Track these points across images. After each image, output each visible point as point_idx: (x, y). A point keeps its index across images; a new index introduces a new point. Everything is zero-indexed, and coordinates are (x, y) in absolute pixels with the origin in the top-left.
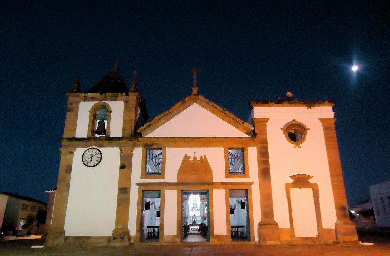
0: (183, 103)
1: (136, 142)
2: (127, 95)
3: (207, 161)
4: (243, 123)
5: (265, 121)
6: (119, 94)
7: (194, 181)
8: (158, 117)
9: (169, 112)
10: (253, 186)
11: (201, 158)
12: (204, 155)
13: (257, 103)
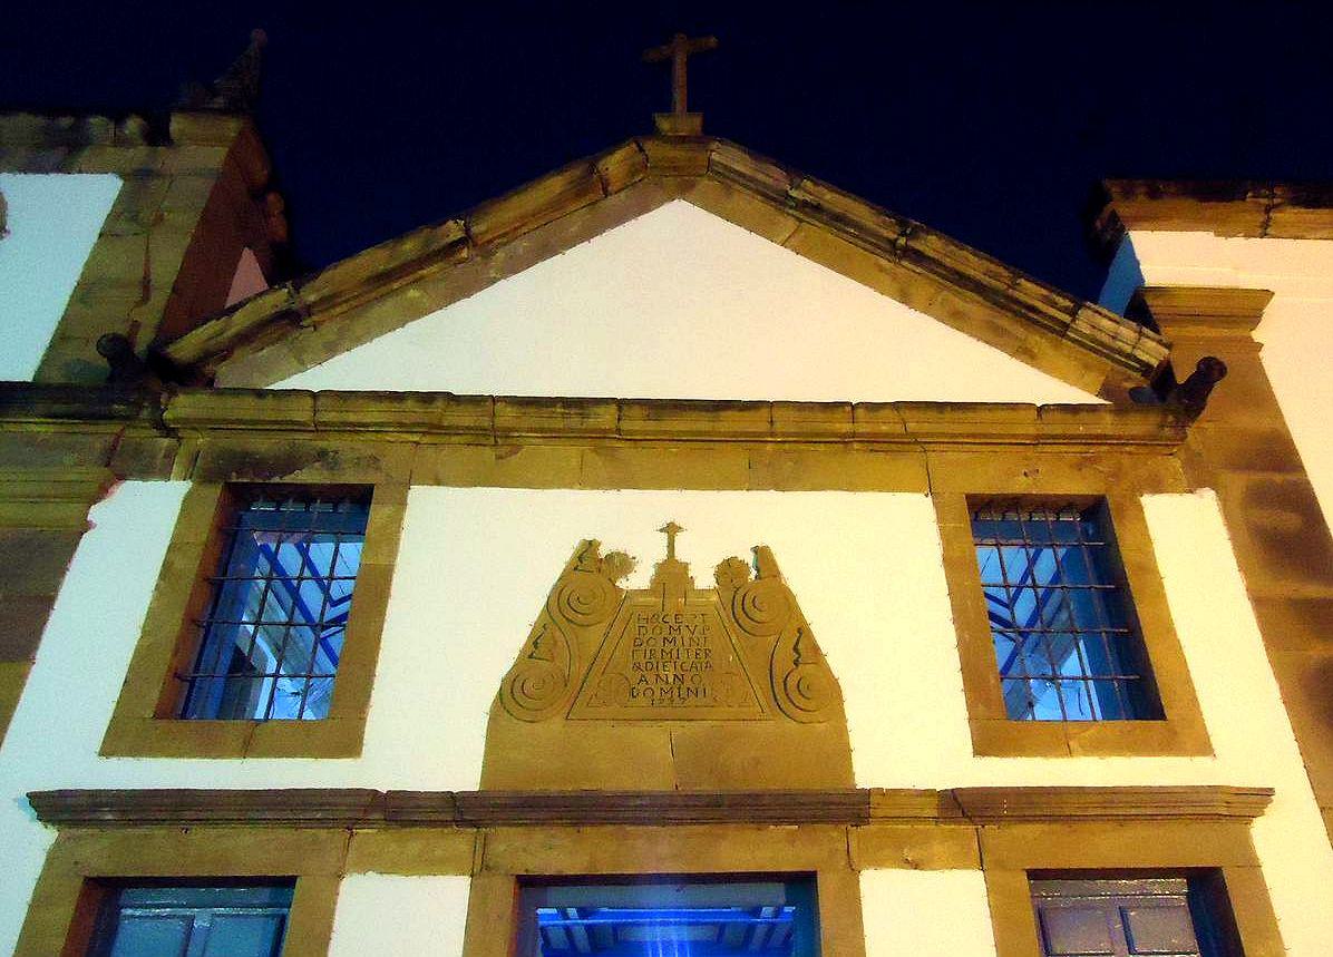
0: (579, 191)
1: (141, 434)
2: (157, 135)
3: (787, 601)
4: (1073, 314)
5: (1244, 308)
6: (97, 123)
7: (659, 781)
8: (373, 259)
9: (467, 230)
10: (1264, 834)
11: (729, 571)
12: (756, 550)
13: (1154, 194)
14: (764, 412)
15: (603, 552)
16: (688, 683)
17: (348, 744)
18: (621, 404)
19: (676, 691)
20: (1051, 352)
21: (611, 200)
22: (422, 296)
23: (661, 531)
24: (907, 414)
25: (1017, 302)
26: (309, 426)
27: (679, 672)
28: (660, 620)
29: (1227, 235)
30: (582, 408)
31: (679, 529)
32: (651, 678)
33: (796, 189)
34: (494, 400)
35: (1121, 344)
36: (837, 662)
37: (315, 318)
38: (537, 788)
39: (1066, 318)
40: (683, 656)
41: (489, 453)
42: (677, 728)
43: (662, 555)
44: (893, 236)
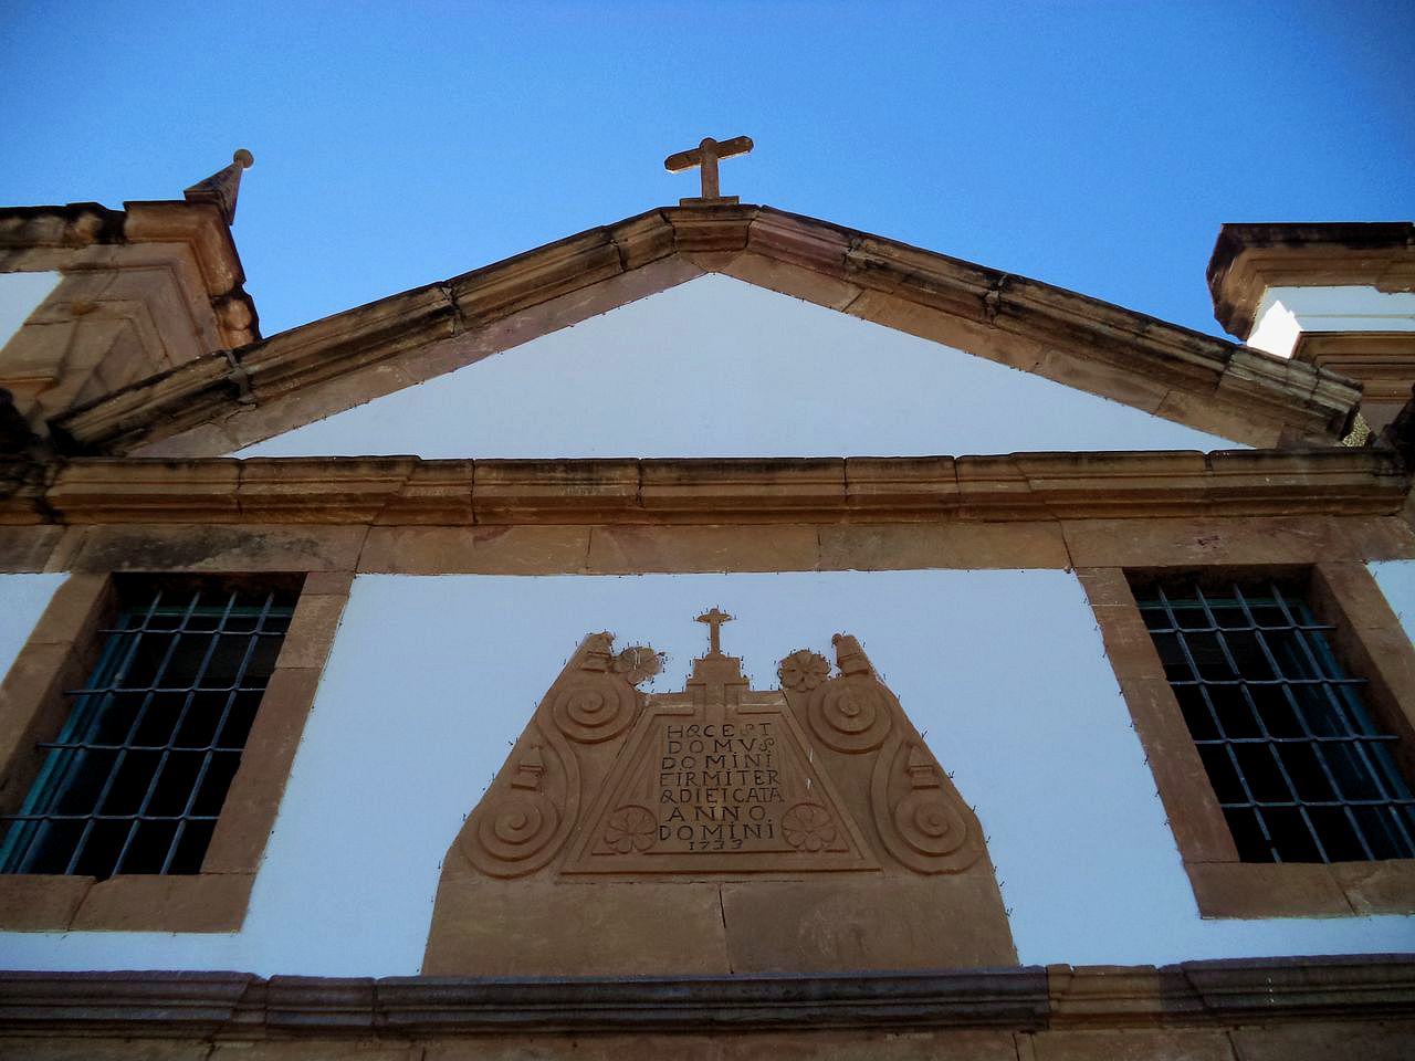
9: (454, 299)
11: (799, 668)
12: (837, 640)
14: (836, 472)
15: (617, 648)
16: (744, 818)
17: (228, 915)
18: (642, 465)
19: (726, 831)
20: (1202, 409)
21: (629, 276)
22: (393, 373)
23: (699, 620)
24: (1027, 467)
25: (1150, 352)
26: (230, 503)
27: (731, 804)
28: (701, 732)
29: (1391, 291)
30: (591, 471)
31: (725, 617)
32: (688, 812)
33: (857, 249)
34: (474, 464)
35: (1295, 390)
36: (970, 790)
37: (259, 394)
38: (513, 975)
39: (1219, 366)
40: (736, 778)
41: (466, 536)
42: (733, 889)
43: (701, 648)
44: (980, 290)
